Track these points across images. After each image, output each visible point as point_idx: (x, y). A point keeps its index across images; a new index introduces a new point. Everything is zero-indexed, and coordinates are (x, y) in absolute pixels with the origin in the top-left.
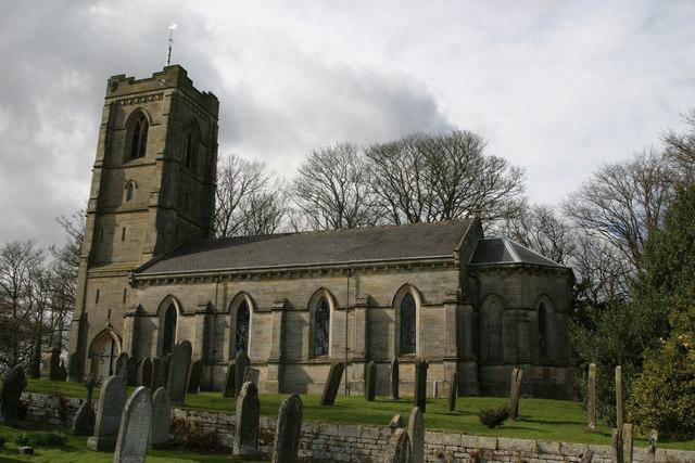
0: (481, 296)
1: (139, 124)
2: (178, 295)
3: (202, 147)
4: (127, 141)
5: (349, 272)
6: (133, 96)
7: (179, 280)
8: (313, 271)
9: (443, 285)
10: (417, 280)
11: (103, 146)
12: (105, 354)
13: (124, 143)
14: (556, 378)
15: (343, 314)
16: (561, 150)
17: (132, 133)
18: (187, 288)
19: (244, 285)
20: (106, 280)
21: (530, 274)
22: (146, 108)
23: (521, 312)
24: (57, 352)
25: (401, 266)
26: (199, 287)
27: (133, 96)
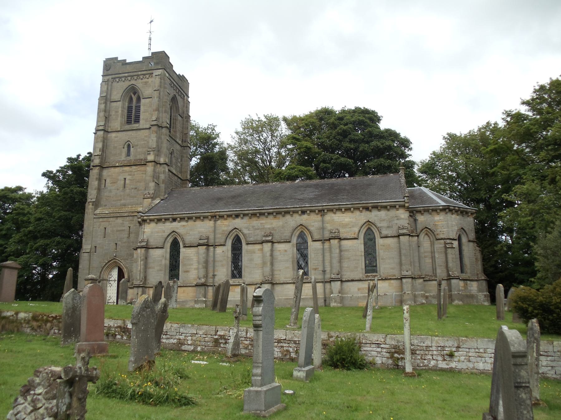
0: (419, 231)
1: (133, 96)
2: (181, 231)
3: (179, 118)
4: (122, 111)
5: (322, 212)
6: (126, 75)
7: (182, 219)
8: (294, 212)
9: (396, 222)
10: (376, 218)
11: (102, 114)
12: (112, 279)
13: (120, 112)
14: (472, 288)
15: (318, 245)
16: (442, 98)
17: (127, 104)
18: (256, 222)
19: (238, 223)
20: (111, 219)
21: (452, 214)
22: (139, 84)
23: (448, 241)
24: (530, 221)
25: (363, 208)
26: (199, 223)
27: (126, 75)
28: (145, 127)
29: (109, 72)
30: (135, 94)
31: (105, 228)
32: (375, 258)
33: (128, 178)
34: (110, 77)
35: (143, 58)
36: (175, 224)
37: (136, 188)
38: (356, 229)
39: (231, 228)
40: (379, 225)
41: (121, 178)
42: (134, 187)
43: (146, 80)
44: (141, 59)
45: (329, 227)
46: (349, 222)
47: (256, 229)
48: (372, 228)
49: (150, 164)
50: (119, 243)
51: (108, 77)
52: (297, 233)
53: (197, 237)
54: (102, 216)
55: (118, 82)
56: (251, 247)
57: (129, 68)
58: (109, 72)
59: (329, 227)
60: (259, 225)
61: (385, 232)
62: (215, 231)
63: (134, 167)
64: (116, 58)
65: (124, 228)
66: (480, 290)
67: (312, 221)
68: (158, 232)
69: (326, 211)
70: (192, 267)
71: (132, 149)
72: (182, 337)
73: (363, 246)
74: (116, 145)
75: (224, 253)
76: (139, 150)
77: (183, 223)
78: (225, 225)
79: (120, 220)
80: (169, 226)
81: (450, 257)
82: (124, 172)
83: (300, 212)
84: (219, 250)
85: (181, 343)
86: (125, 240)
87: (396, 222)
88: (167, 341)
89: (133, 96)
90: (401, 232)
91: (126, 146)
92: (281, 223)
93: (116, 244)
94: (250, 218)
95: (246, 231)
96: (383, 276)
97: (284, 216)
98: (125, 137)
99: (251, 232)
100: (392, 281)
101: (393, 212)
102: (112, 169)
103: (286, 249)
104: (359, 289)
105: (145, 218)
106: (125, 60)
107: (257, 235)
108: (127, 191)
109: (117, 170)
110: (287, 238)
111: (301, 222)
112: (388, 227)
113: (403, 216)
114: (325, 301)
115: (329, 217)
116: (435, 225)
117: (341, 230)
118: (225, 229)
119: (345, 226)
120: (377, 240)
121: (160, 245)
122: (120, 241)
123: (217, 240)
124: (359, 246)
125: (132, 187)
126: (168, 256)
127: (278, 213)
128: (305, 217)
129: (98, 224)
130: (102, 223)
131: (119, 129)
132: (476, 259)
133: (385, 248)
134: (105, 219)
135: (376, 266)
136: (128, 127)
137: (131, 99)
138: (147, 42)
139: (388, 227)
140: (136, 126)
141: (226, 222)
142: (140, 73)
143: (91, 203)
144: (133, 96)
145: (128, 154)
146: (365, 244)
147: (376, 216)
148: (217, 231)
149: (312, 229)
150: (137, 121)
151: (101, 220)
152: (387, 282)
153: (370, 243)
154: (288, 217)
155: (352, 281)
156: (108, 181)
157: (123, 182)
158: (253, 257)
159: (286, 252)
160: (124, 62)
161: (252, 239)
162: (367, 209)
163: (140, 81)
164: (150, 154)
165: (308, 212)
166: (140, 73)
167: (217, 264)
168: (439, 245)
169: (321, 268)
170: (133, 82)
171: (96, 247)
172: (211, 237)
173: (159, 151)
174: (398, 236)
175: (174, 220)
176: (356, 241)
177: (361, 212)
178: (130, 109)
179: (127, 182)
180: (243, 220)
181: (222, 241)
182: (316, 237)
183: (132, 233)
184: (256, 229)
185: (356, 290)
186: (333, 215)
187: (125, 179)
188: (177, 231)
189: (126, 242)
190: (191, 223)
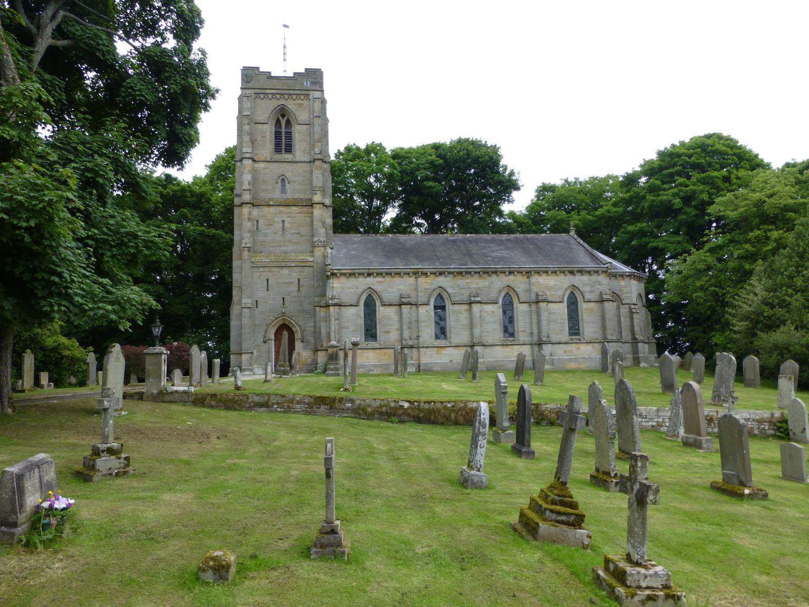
2: (377, 287)
5: (528, 274)
7: (380, 274)
19: (442, 281)
20: (275, 269)
22: (291, 105)
26: (397, 280)
27: (274, 91)
28: (303, 159)
29: (250, 85)
30: (283, 116)
31: (268, 280)
32: (578, 321)
33: (287, 220)
34: (253, 91)
35: (295, 74)
36: (370, 280)
37: (298, 234)
38: (561, 293)
39: (433, 287)
40: (582, 290)
41: (278, 219)
42: (296, 231)
43: (300, 101)
44: (292, 75)
45: (535, 289)
46: (554, 285)
47: (461, 289)
48: (443, 294)
49: (318, 206)
50: (287, 297)
51: (248, 91)
52: (435, 295)
53: (397, 294)
54: (263, 264)
55: (262, 99)
56: (457, 307)
57: (270, 84)
58: (250, 85)
59: (535, 289)
60: (464, 284)
61: (588, 296)
62: (416, 289)
63: (294, 208)
64: (258, 68)
65: (292, 280)
66: (650, 353)
67: (519, 283)
68: (349, 288)
69: (533, 273)
70: (393, 327)
71: (288, 186)
72: (660, 420)
73: (566, 309)
74: (266, 178)
75: (427, 313)
76: (297, 187)
77: (380, 279)
78: (427, 284)
79: (285, 271)
80: (363, 283)
81: (636, 321)
82: (281, 212)
83: (507, 273)
84: (422, 310)
85: (660, 425)
86: (295, 294)
87: (599, 287)
88: (647, 424)
89: (281, 119)
90: (404, 300)
91: (279, 181)
92: (487, 284)
93: (283, 299)
94: (455, 276)
95: (450, 290)
96: (587, 339)
97: (490, 276)
98: (277, 169)
99: (456, 291)
100: (595, 345)
101: (594, 278)
102: (266, 209)
103: (493, 310)
104: (565, 352)
105: (335, 271)
106: (270, 73)
107: (463, 295)
108: (288, 236)
109: (272, 209)
110: (494, 299)
111: (508, 283)
112: (591, 292)
113: (604, 282)
114: (533, 363)
115: (535, 278)
116: (621, 290)
117: (548, 293)
118: (428, 287)
119: (550, 288)
120: (579, 304)
121: (354, 302)
122: (288, 295)
123: (419, 299)
124: (562, 309)
125: (293, 231)
126: (362, 315)
127: (487, 273)
128: (511, 277)
129: (258, 274)
130: (264, 273)
131: (269, 159)
132: (648, 323)
133: (588, 313)
134: (267, 269)
135: (578, 329)
136: (278, 157)
137: (278, 122)
138: (287, 57)
139: (591, 292)
140: (288, 156)
141: (428, 280)
142: (292, 92)
143: (246, 249)
144: (281, 119)
145: (283, 190)
146: (568, 307)
147: (579, 280)
148: (419, 289)
149: (519, 290)
150: (289, 149)
151: (261, 269)
152: (590, 345)
153: (572, 307)
154: (494, 277)
155: (559, 343)
156: (261, 222)
157: (280, 225)
158: (456, 316)
159: (492, 314)
160: (268, 75)
161: (457, 299)
162: (572, 273)
163: (292, 101)
164: (316, 194)
165: (516, 273)
166: (292, 92)
167: (421, 325)
168: (624, 310)
169: (528, 331)
170: (282, 102)
171: (257, 301)
172: (413, 295)
173: (324, 191)
174: (400, 305)
175: (369, 275)
176: (561, 304)
177: (565, 275)
178: (278, 134)
179: (287, 225)
180: (447, 279)
181: (425, 300)
182: (523, 299)
183: (302, 286)
184: (461, 289)
185: (562, 352)
186: (539, 277)
187: (283, 221)
188: (374, 287)
189: (295, 297)
190: (388, 278)
